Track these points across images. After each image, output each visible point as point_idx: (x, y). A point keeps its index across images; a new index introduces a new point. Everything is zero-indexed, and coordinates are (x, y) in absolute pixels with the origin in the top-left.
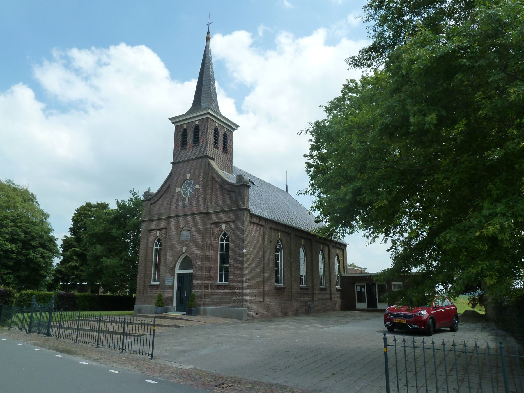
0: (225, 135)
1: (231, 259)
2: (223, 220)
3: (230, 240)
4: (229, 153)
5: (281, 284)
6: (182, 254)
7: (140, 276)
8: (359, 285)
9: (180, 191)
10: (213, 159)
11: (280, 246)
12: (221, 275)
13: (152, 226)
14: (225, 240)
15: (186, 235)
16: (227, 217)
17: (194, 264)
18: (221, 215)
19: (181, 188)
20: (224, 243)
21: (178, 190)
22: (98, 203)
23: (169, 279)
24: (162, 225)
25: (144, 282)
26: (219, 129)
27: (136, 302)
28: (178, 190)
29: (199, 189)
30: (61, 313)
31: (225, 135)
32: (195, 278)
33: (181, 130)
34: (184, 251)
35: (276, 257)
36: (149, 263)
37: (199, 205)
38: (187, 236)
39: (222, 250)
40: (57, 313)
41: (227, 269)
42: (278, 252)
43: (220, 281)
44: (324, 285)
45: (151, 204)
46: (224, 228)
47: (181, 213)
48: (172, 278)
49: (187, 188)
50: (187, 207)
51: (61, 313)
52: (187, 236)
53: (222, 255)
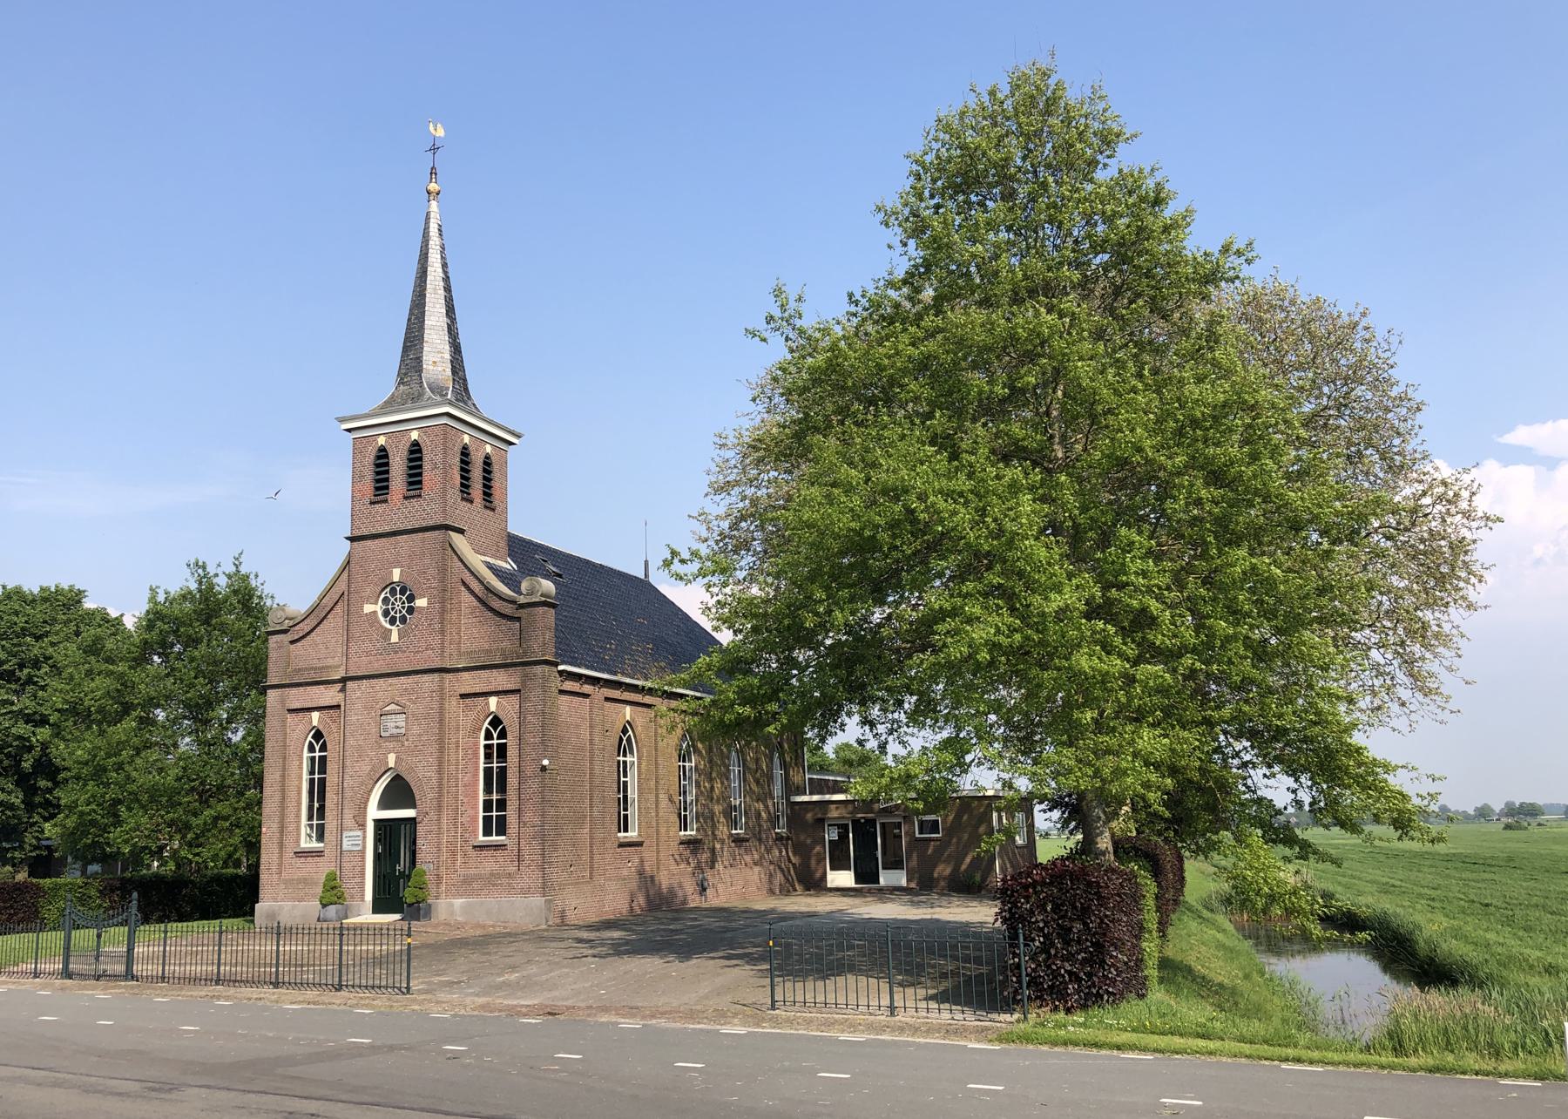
0: (487, 462)
1: (512, 780)
2: (491, 688)
3: (509, 736)
4: (498, 509)
5: (633, 834)
6: (386, 772)
7: (269, 831)
8: (834, 825)
9: (375, 612)
10: (461, 531)
11: (629, 739)
12: (487, 820)
13: (297, 698)
14: (495, 736)
15: (395, 724)
16: (501, 679)
17: (417, 797)
18: (484, 674)
19: (376, 603)
20: (495, 742)
21: (368, 608)
22: (671, 891)
23: (351, 834)
24: (330, 695)
25: (281, 845)
26: (472, 449)
27: (261, 896)
28: (368, 608)
29: (428, 608)
30: (166, 927)
31: (487, 462)
32: (421, 830)
33: (371, 453)
34: (391, 764)
35: (619, 767)
36: (292, 795)
37: (427, 649)
38: (397, 727)
39: (488, 756)
40: (157, 929)
41: (502, 805)
42: (625, 756)
43: (484, 835)
44: (741, 829)
45: (292, 642)
46: (493, 708)
47: (379, 666)
48: (359, 833)
49: (393, 604)
50: (396, 652)
51: (166, 927)
52: (397, 727)
53: (488, 772)
